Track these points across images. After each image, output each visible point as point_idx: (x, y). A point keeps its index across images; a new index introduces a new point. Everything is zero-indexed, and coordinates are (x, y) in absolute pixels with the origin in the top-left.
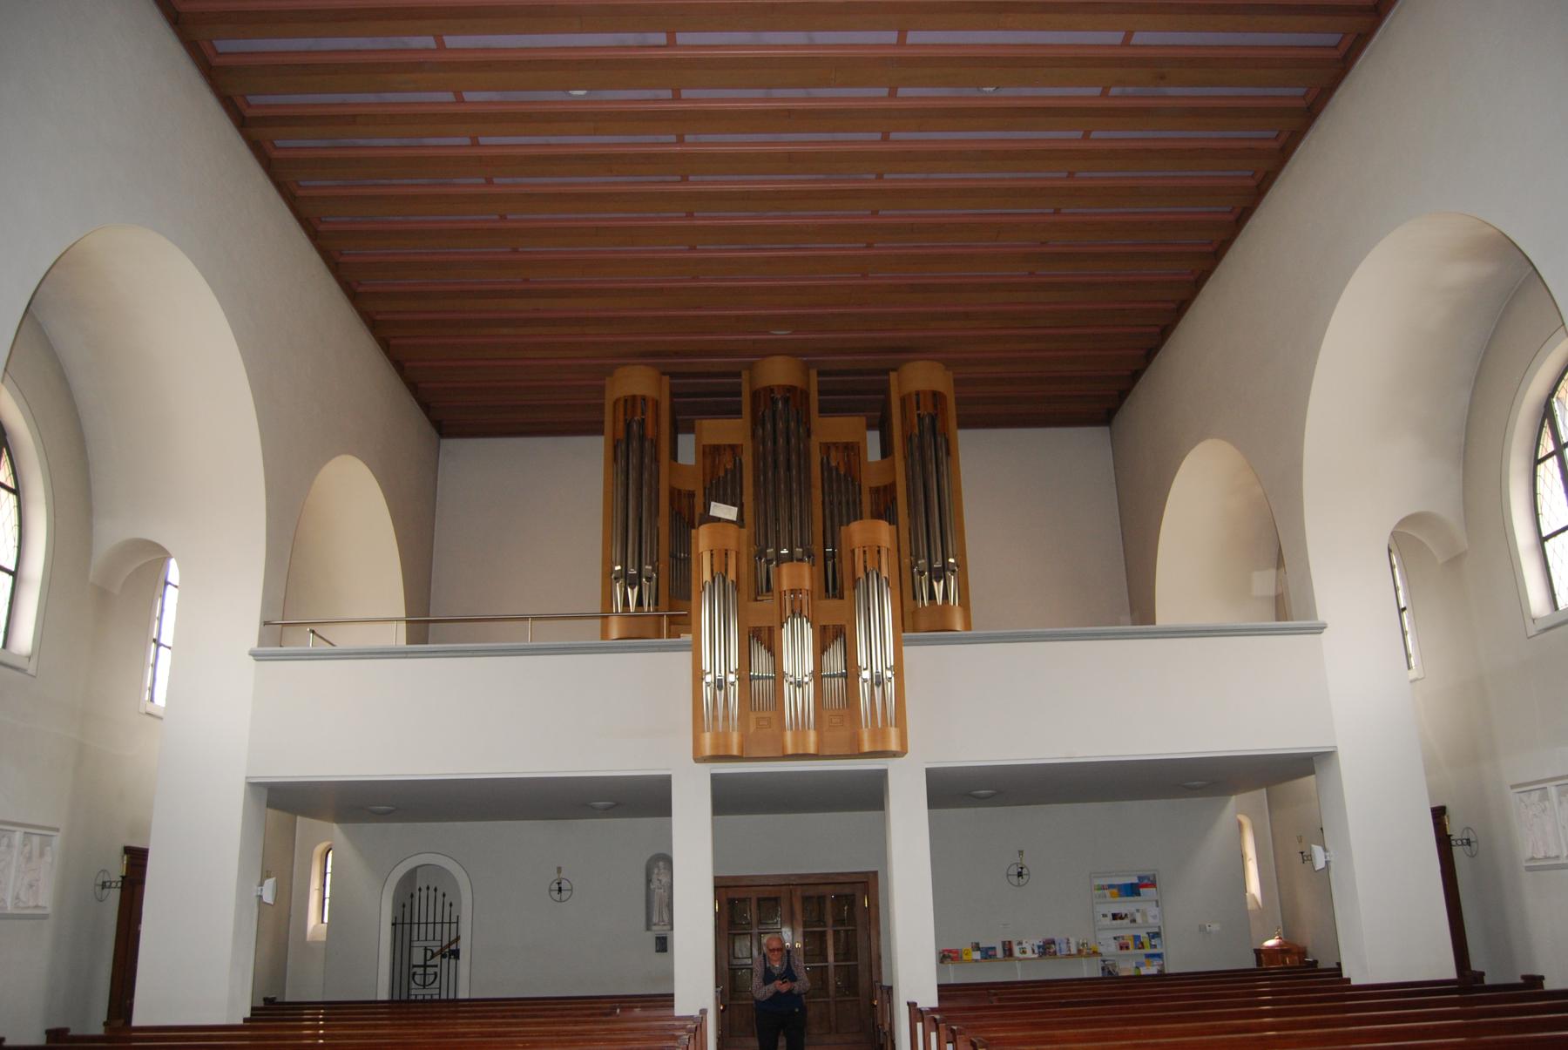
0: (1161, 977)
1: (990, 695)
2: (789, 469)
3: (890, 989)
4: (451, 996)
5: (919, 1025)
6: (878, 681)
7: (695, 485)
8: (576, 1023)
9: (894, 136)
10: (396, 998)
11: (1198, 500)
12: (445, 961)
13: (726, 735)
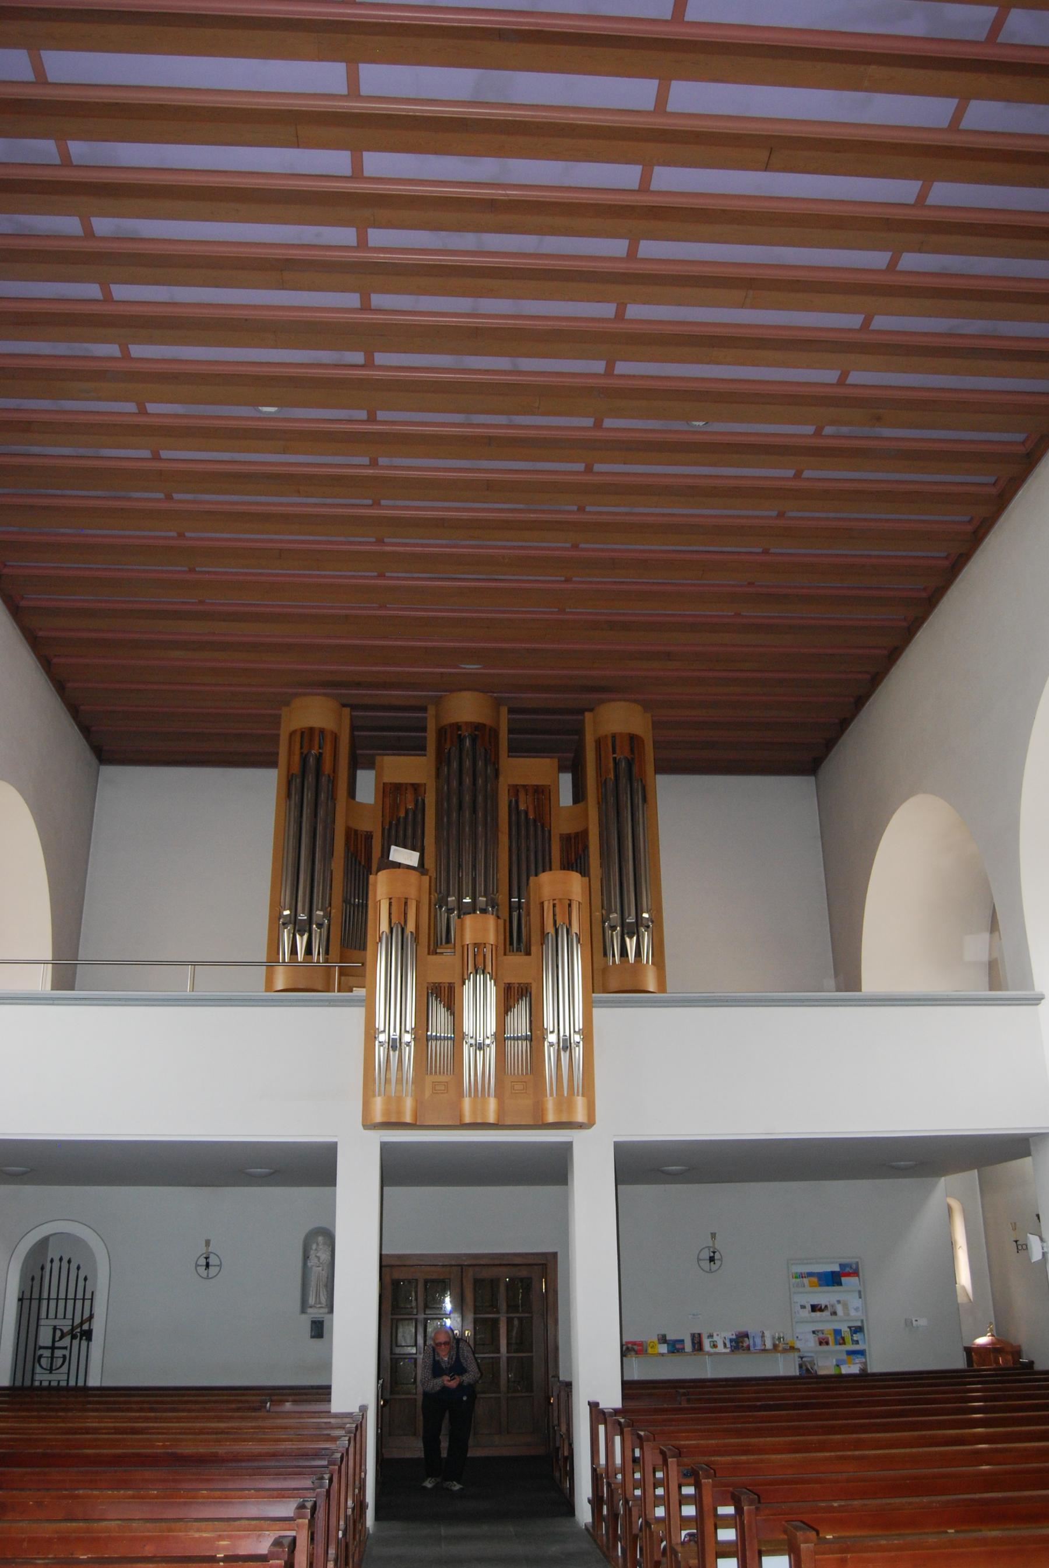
0: (864, 1376)
1: (684, 1061)
2: (474, 810)
3: (569, 1385)
4: (81, 1383)
5: (602, 1428)
6: (566, 1045)
7: (371, 825)
8: (220, 1419)
9: (598, 467)
10: (18, 1383)
11: (907, 859)
12: (76, 1342)
13: (399, 1099)
